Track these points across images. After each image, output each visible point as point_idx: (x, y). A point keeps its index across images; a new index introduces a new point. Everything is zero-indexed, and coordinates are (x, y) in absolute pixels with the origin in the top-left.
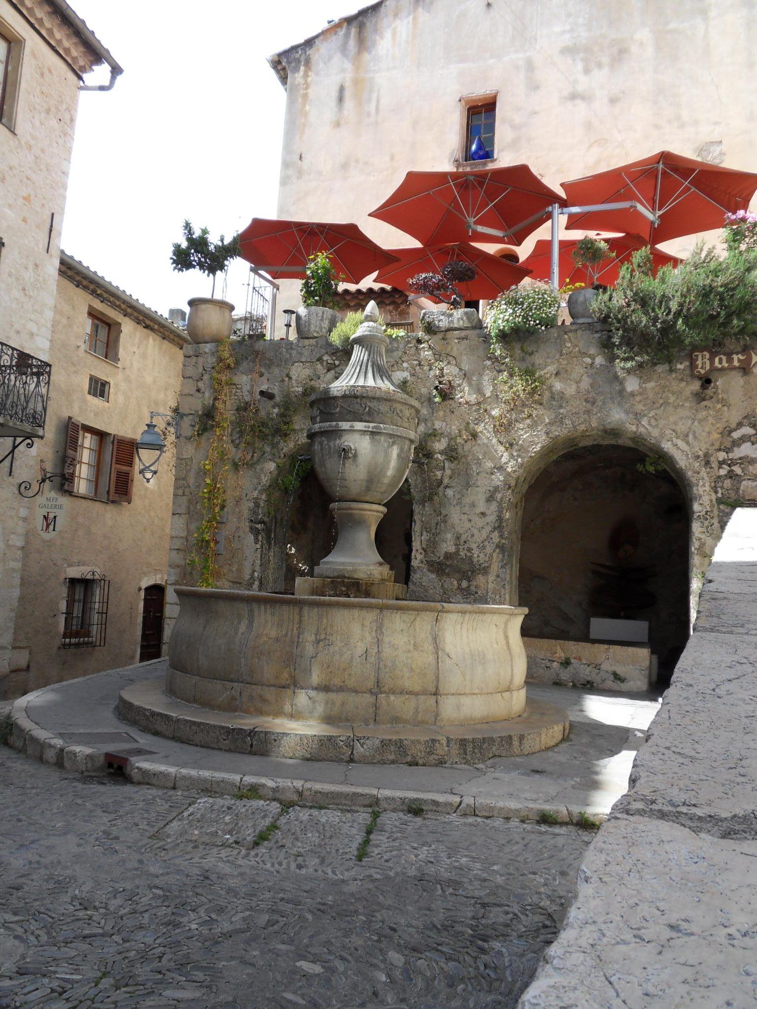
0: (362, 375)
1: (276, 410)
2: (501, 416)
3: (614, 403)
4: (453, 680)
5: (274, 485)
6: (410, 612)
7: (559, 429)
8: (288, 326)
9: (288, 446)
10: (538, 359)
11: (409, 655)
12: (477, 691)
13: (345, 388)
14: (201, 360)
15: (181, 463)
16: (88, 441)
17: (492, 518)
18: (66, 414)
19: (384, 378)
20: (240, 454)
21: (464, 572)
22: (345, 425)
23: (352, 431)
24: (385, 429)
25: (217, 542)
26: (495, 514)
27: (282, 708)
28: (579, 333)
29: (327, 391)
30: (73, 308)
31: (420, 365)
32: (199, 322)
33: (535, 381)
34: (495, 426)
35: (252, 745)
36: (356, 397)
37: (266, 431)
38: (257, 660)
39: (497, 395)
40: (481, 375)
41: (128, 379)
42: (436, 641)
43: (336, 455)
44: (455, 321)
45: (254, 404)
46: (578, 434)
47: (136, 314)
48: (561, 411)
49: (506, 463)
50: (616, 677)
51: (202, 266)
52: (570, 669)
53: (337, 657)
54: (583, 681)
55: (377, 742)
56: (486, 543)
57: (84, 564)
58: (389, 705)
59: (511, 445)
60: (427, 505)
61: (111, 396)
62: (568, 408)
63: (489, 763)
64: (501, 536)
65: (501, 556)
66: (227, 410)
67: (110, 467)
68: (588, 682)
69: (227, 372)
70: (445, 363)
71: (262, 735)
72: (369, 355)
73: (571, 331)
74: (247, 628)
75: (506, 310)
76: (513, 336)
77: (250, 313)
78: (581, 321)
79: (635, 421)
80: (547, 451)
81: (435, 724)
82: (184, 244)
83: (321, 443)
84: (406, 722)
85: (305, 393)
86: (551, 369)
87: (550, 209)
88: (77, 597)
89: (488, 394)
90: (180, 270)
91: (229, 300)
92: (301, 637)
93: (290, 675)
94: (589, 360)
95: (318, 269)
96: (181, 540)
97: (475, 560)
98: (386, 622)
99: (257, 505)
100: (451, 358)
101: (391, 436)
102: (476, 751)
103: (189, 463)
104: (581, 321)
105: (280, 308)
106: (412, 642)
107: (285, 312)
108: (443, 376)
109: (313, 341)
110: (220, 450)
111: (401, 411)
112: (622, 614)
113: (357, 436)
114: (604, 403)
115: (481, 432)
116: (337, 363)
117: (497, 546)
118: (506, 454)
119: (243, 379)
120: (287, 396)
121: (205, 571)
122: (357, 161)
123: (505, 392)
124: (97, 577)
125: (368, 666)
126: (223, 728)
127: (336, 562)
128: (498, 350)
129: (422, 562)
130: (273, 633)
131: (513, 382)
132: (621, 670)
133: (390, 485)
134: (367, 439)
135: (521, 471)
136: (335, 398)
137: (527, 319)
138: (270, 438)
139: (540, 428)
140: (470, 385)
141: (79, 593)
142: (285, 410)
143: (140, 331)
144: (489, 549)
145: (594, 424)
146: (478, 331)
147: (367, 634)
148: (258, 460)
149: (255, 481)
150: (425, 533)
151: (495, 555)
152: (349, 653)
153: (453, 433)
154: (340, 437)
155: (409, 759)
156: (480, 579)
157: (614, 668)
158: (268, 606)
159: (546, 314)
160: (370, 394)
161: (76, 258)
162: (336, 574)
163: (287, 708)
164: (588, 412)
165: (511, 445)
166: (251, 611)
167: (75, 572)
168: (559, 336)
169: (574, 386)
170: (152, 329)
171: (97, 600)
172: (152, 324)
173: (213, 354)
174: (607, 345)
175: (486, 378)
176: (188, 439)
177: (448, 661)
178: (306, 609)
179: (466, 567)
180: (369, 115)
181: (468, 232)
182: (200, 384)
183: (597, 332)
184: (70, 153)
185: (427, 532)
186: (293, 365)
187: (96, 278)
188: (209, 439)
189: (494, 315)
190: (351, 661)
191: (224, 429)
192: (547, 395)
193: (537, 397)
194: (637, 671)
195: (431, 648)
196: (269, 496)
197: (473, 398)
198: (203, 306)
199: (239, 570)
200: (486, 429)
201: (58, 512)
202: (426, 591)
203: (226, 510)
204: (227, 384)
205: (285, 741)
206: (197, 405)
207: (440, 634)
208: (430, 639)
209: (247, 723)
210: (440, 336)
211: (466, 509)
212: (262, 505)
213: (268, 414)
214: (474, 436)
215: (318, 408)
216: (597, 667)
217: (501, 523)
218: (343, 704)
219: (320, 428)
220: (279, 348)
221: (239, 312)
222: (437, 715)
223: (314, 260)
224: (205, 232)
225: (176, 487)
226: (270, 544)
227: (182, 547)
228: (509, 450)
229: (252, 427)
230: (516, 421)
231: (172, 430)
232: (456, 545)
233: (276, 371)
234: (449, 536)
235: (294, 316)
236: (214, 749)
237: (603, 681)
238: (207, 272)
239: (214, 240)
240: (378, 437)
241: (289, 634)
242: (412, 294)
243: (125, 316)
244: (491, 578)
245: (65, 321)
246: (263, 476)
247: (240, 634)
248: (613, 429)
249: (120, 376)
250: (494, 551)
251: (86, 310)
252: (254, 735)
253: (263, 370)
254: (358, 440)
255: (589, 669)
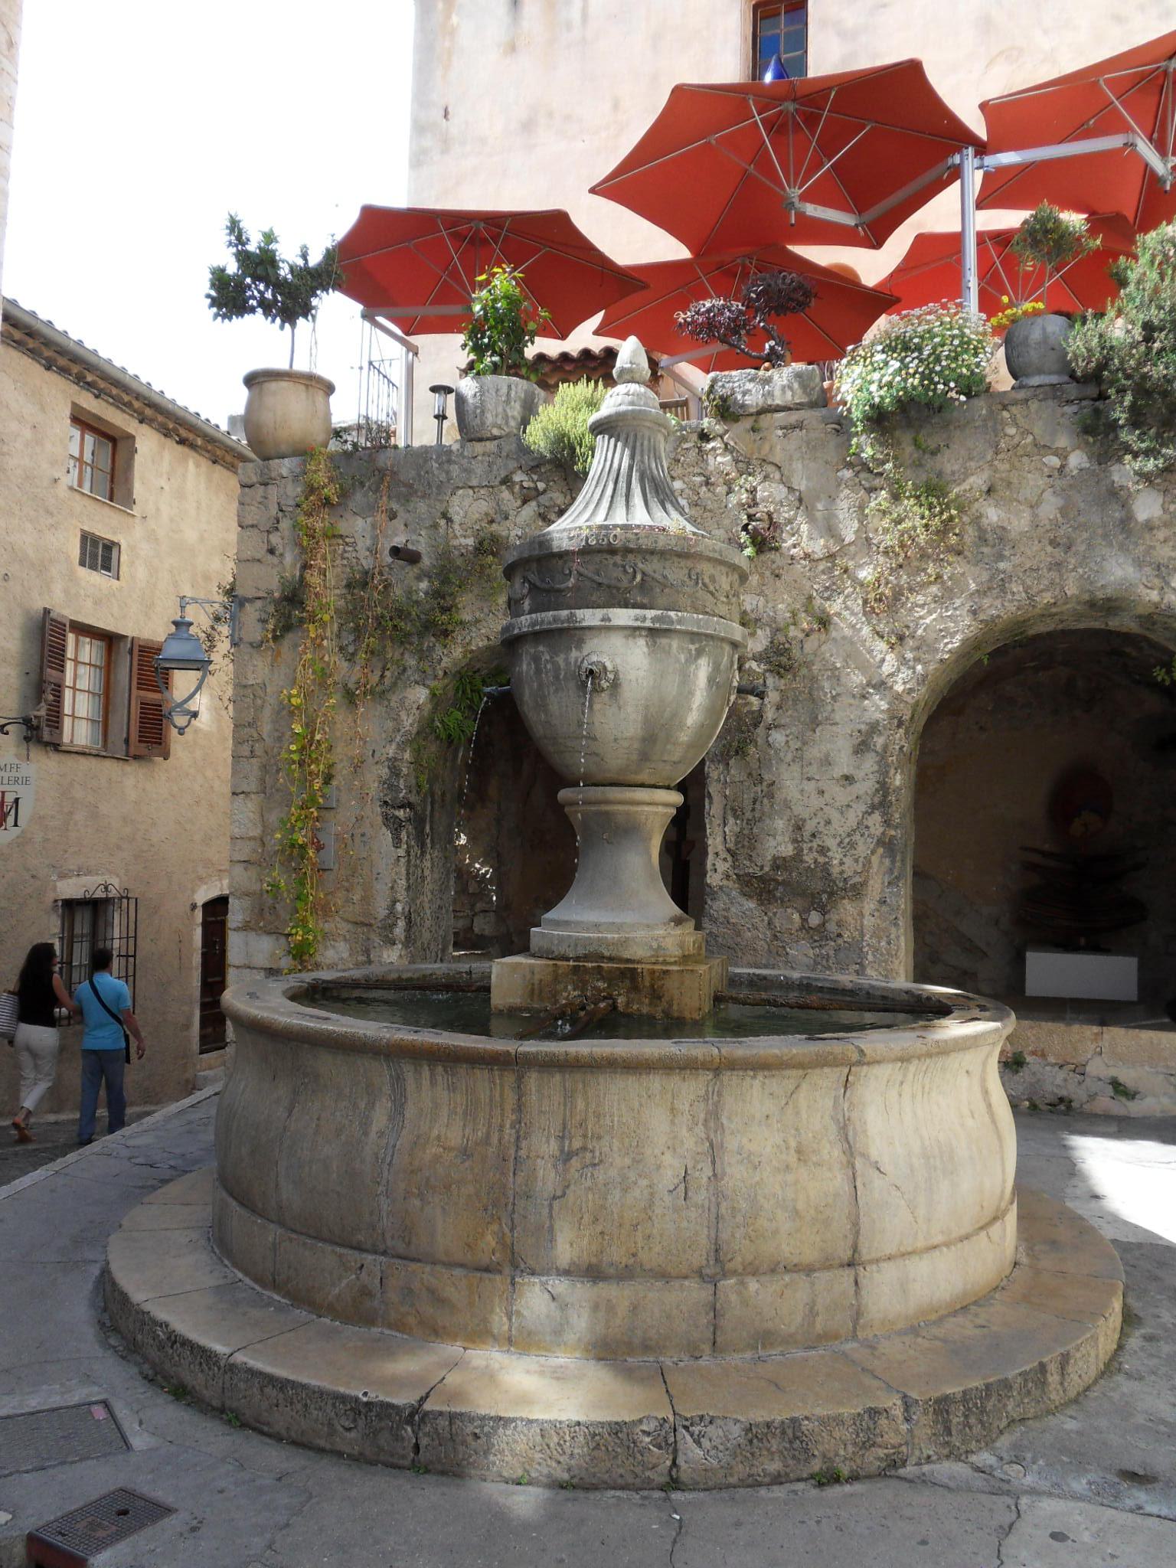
0: (620, 501)
1: (424, 585)
2: (878, 580)
3: (1111, 545)
4: (890, 1225)
5: (426, 729)
6: (787, 1072)
7: (998, 603)
8: (441, 417)
9: (452, 655)
10: (948, 463)
11: (790, 1178)
12: (939, 1239)
13: (585, 532)
14: (273, 492)
15: (244, 693)
16: (82, 654)
17: (866, 786)
18: (39, 604)
19: (669, 506)
20: (357, 674)
21: (812, 895)
22: (590, 617)
23: (607, 628)
24: (680, 621)
25: (319, 848)
26: (873, 778)
27: (485, 1320)
28: (1034, 405)
29: (543, 542)
30: (43, 409)
31: (707, 483)
32: (267, 418)
33: (948, 508)
34: (865, 602)
35: (417, 1448)
36: (612, 551)
37: (406, 626)
38: (417, 1202)
39: (867, 539)
40: (832, 499)
41: (152, 537)
42: (846, 1133)
43: (572, 685)
44: (777, 393)
45: (381, 574)
46: (1038, 611)
47: (160, 418)
48: (1002, 565)
49: (892, 675)
50: (1118, 1088)
51: (267, 307)
52: (1024, 1074)
53: (616, 1194)
54: (1050, 1098)
55: (736, 1431)
56: (857, 837)
57: (89, 873)
58: (745, 1303)
59: (901, 638)
60: (732, 762)
61: (124, 569)
62: (1016, 560)
63: (1004, 1442)
64: (887, 823)
65: (887, 861)
66: (328, 590)
67: (129, 699)
68: (1061, 1100)
69: (325, 513)
70: (759, 478)
71: (443, 1423)
72: (632, 457)
73: (1015, 403)
74: (391, 1119)
75: (886, 363)
76: (904, 418)
77: (367, 418)
78: (1035, 381)
79: (1157, 581)
80: (972, 646)
81: (854, 1337)
82: (232, 268)
83: (536, 659)
84: (789, 1340)
85: (480, 549)
86: (977, 481)
87: (957, 159)
88: (77, 931)
89: (849, 536)
90: (224, 317)
91: (323, 371)
92: (524, 1144)
93: (502, 1242)
94: (1055, 461)
95: (495, 301)
96: (252, 843)
97: (835, 871)
98: (729, 1101)
99: (395, 772)
100: (770, 468)
101: (694, 636)
102: (972, 1420)
103: (260, 693)
104: (1035, 381)
105: (422, 393)
106: (793, 1144)
107: (435, 389)
108: (756, 504)
109: (491, 446)
110: (318, 666)
111: (713, 579)
112: (1083, 941)
113: (617, 641)
114: (1090, 546)
115: (838, 614)
116: (541, 486)
117: (880, 842)
118: (890, 658)
119: (357, 526)
120: (445, 555)
121: (299, 905)
122: (550, 115)
123: (886, 531)
124: (113, 893)
125: (693, 1214)
126: (343, 1398)
127: (577, 923)
128: (867, 448)
129: (728, 877)
130: (455, 1136)
131: (900, 509)
132: (1127, 1076)
133: (691, 746)
134: (640, 646)
135: (923, 690)
136: (564, 555)
137: (931, 380)
138: (415, 639)
139: (958, 602)
140: (811, 519)
141: (82, 924)
142: (443, 583)
143: (171, 451)
144: (863, 849)
145: (1072, 590)
146: (824, 411)
147: (684, 1132)
148: (395, 684)
149: (390, 724)
150: (731, 821)
151: (875, 860)
152: (644, 1182)
153: (779, 619)
154: (580, 644)
155: (816, 1465)
156: (847, 909)
157: (1113, 1072)
158: (440, 1069)
159: (968, 367)
160: (645, 543)
161: (101, 354)
162: (581, 952)
163: (499, 1322)
164: (1058, 566)
165: (901, 638)
166: (398, 1080)
167: (72, 888)
168: (991, 412)
169: (1026, 515)
170: (193, 446)
171: (116, 935)
172: (191, 436)
173: (296, 478)
174: (1097, 431)
175: (844, 504)
176: (257, 646)
177: (878, 1182)
178: (532, 1079)
179: (817, 885)
180: (569, 26)
181: (788, 217)
182: (275, 539)
183: (1069, 402)
184: (11, 109)
185: (736, 817)
186: (453, 494)
187: (81, 352)
188: (296, 646)
189: (862, 378)
190: (651, 1204)
191: (323, 625)
192: (971, 533)
193: (953, 540)
194: (1161, 1077)
195: (836, 1152)
196: (417, 752)
197: (818, 546)
198: (273, 386)
199: (366, 899)
200: (847, 608)
201: (22, 791)
202: (738, 934)
203: (334, 783)
204: (326, 536)
205: (503, 1438)
206: (269, 579)
207: (854, 1115)
208: (833, 1129)
209: (400, 1373)
210: (747, 423)
211: (812, 771)
212: (405, 771)
213: (409, 592)
214: (824, 622)
215: (525, 579)
216: (1080, 1070)
217: (885, 796)
218: (634, 1309)
219: (534, 624)
220: (426, 461)
221: (344, 411)
222: (858, 1314)
223: (484, 285)
224: (269, 237)
225: (238, 742)
226: (423, 846)
227: (254, 857)
228: (898, 648)
229: (379, 619)
230: (911, 590)
231: (225, 629)
232: (795, 841)
233: (422, 507)
234: (780, 824)
235: (451, 397)
236: (321, 1451)
237: (1092, 1097)
238: (278, 320)
239: (288, 254)
240: (664, 641)
241: (495, 1140)
242: (665, 357)
243: (141, 422)
244: (869, 905)
245: (28, 434)
246: (403, 715)
247: (373, 1135)
248: (1109, 599)
249: (138, 531)
250: (873, 853)
251: (68, 412)
252: (422, 1420)
253: (395, 506)
254: (621, 649)
255: (1061, 1075)
